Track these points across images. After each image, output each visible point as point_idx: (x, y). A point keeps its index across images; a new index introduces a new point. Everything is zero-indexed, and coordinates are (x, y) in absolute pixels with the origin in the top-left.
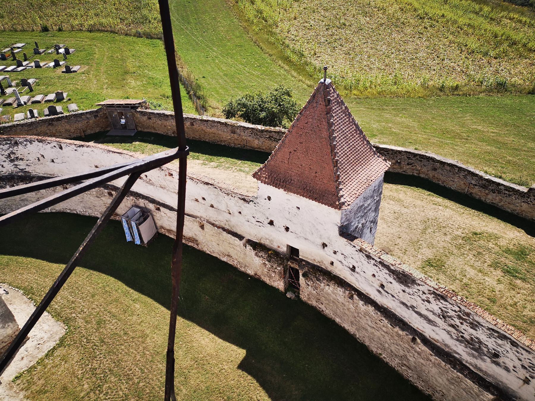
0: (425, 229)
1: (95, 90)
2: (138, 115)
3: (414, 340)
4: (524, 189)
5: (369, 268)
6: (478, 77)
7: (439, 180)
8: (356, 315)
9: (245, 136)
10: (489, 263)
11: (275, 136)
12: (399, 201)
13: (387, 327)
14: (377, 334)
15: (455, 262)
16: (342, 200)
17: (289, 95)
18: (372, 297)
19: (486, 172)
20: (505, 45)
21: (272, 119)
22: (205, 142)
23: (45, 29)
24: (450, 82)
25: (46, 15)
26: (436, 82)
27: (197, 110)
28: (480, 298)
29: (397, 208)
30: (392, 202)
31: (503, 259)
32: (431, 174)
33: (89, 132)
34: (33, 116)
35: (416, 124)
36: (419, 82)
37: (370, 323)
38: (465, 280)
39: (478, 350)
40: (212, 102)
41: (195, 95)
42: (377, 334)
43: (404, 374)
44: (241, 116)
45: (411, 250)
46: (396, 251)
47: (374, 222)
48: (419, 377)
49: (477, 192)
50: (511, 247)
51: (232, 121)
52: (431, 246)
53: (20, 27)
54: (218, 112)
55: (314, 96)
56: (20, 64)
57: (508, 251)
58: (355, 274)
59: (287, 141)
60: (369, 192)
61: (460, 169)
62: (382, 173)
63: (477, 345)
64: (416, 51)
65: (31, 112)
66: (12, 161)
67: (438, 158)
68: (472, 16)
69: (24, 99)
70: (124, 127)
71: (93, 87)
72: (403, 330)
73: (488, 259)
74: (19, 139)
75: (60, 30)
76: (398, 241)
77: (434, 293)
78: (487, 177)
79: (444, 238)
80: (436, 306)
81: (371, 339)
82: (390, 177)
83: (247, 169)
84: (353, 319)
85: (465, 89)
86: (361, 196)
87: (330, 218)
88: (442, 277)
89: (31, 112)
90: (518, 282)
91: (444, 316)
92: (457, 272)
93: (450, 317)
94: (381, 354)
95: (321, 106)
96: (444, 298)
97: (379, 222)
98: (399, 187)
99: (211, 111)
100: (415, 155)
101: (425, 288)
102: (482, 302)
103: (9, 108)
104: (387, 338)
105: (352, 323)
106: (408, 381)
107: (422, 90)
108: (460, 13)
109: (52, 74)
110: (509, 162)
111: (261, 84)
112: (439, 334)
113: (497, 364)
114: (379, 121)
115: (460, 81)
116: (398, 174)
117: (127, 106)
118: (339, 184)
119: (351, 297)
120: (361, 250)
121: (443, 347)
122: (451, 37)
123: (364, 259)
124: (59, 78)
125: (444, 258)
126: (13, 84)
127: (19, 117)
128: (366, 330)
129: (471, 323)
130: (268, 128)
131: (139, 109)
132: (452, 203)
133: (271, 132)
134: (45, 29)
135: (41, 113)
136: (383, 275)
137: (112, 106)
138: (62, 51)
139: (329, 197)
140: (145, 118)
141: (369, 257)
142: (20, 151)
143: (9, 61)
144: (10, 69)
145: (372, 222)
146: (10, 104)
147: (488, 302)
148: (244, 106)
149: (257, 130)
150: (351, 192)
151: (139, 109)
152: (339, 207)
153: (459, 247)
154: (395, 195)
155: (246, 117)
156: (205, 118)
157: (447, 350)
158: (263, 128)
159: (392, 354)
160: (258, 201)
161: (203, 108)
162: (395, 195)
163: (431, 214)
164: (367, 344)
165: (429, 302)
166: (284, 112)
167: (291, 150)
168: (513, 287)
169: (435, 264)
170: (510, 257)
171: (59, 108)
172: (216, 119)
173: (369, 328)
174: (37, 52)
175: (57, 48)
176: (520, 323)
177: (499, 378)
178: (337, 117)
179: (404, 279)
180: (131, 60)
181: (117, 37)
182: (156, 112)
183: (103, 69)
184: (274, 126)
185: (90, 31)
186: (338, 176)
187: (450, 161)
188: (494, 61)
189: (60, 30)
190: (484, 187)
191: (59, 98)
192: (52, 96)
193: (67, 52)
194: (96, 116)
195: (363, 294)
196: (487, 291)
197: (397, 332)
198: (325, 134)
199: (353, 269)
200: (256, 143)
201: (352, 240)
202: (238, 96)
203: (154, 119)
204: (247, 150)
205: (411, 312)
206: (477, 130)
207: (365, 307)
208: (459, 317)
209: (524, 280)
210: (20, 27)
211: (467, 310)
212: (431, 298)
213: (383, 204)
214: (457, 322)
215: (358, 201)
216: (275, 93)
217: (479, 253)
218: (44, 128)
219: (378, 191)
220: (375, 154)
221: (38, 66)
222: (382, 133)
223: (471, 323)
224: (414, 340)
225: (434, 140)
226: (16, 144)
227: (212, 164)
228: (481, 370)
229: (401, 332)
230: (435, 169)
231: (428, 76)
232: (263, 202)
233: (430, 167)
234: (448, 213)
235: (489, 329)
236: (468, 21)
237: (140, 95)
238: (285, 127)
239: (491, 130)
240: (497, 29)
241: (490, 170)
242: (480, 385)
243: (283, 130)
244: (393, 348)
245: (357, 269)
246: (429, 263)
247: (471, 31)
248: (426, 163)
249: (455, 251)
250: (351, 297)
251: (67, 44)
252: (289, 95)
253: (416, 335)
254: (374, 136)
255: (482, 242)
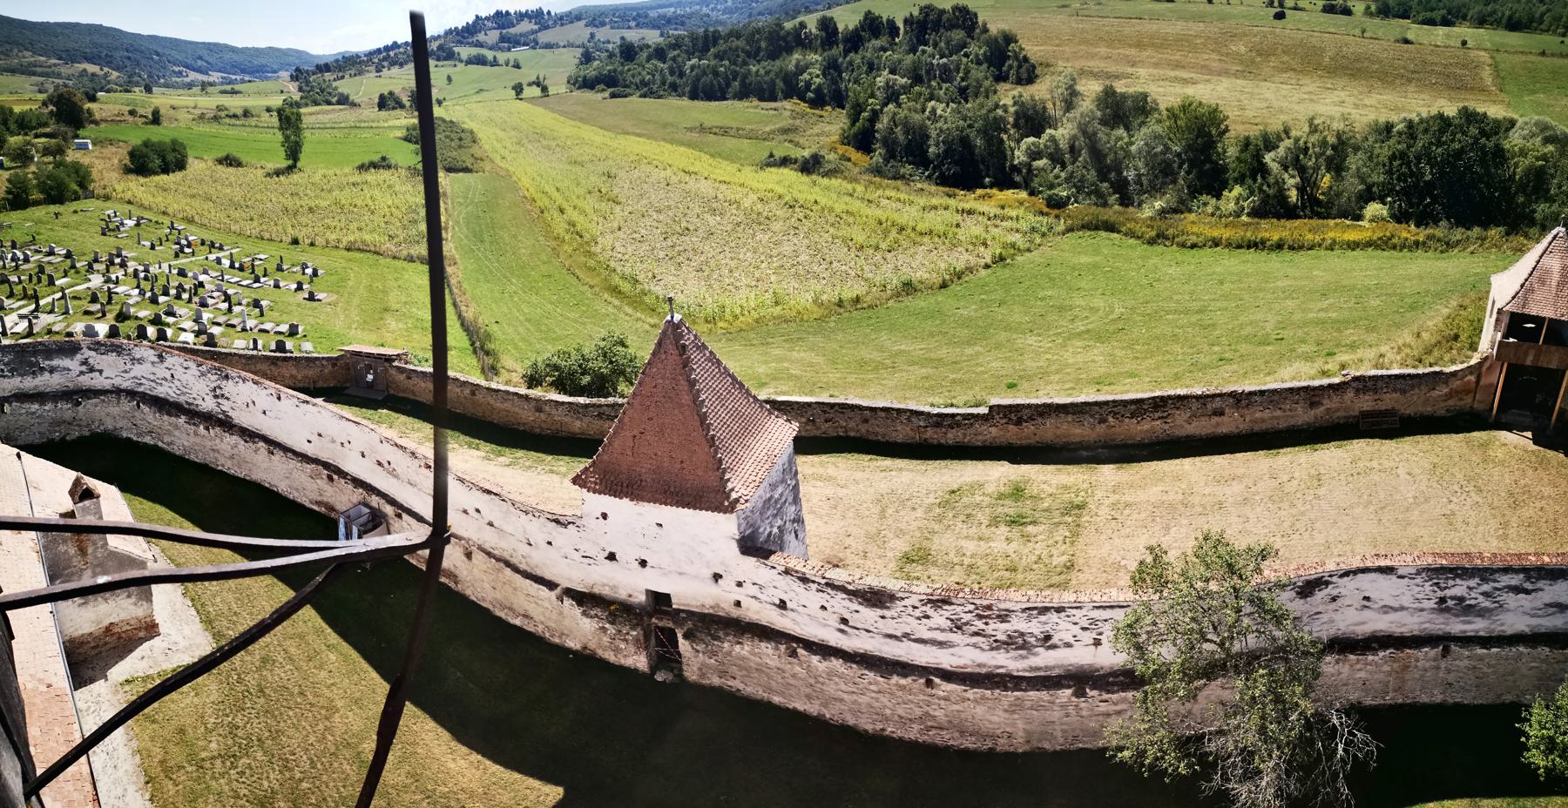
0: (883, 511)
1: (335, 330)
2: (393, 372)
3: (929, 683)
4: (984, 410)
5: (812, 598)
6: (878, 279)
7: (876, 434)
8: (812, 681)
9: (559, 415)
10: (986, 522)
11: (608, 411)
12: (829, 479)
13: (876, 683)
14: (864, 700)
15: (943, 543)
16: (734, 496)
17: (624, 345)
18: (833, 643)
19: (932, 405)
20: (894, 234)
21: (601, 386)
22: (491, 424)
23: (295, 242)
24: (848, 294)
25: (300, 224)
26: (829, 296)
27: (483, 371)
28: (996, 575)
29: (830, 491)
30: (819, 484)
31: (1000, 509)
32: (863, 428)
33: (320, 384)
34: (255, 348)
35: (820, 360)
36: (809, 297)
37: (843, 687)
38: (967, 561)
39: (1025, 646)
40: (507, 361)
41: (482, 348)
42: (864, 700)
43: (938, 740)
44: (551, 384)
45: (873, 550)
46: (851, 559)
47: (798, 520)
48: (962, 733)
49: (931, 434)
50: (1002, 489)
51: (536, 392)
52: (900, 533)
53: (267, 236)
54: (516, 378)
55: (659, 344)
56: (257, 280)
57: (1001, 496)
58: (789, 613)
59: (626, 419)
60: (775, 475)
61: (899, 411)
62: (790, 441)
63: (1020, 641)
64: (796, 254)
65: (255, 341)
66: (216, 397)
67: (865, 403)
68: (848, 199)
69: (250, 323)
70: (370, 385)
71: (338, 325)
72: (905, 676)
73: (983, 517)
74: (232, 372)
75: (312, 244)
76: (848, 541)
77: (930, 601)
78: (936, 411)
79: (914, 515)
80: (940, 618)
81: (856, 712)
82: (803, 445)
83: (563, 469)
84: (808, 690)
85: (868, 298)
86: (765, 484)
87: (719, 530)
88: (933, 571)
89: (255, 341)
90: (1030, 528)
91: (958, 627)
92: (952, 555)
93: (966, 624)
94: (883, 730)
95: (673, 357)
96: (946, 602)
97: (807, 517)
98: (824, 458)
99: (504, 375)
100: (832, 406)
101: (914, 600)
102: (1000, 579)
103: (231, 330)
104: (885, 700)
105: (809, 697)
106: (948, 748)
107: (816, 309)
108: (834, 196)
109: (291, 300)
110: (954, 381)
111: (580, 333)
112: (965, 655)
113: (1054, 647)
114: (766, 362)
115: (858, 289)
116: (815, 438)
117: (380, 357)
118: (724, 471)
119: (793, 654)
120: (787, 572)
121: (978, 670)
122: (832, 230)
123: (798, 587)
124: (299, 305)
125: (925, 543)
126: (244, 302)
127: (240, 344)
128: (842, 700)
129: (999, 616)
130: (595, 400)
131: (396, 364)
132: (906, 461)
133: (600, 406)
134: (295, 242)
135: (266, 345)
136: (840, 604)
137: (358, 354)
138: (309, 271)
139: (712, 497)
140: (402, 377)
141: (804, 580)
142: (229, 387)
143: (246, 274)
144: (245, 283)
145: (794, 521)
146: (233, 326)
147: (1007, 574)
148: (556, 367)
149: (577, 405)
150: (747, 479)
151: (396, 364)
152: (731, 509)
153: (940, 519)
154: (821, 471)
155: (560, 385)
156: (494, 386)
157: (984, 671)
158: (588, 401)
159: (904, 721)
160: (583, 522)
161: (492, 370)
162: (821, 471)
163: (883, 487)
164: (851, 721)
165: (927, 617)
166: (619, 372)
167: (636, 432)
168: (1027, 538)
169: (916, 558)
170: (1007, 502)
171: (289, 345)
172: (512, 389)
173: (845, 696)
174: (280, 269)
175: (304, 266)
176: (1056, 579)
177: (1066, 662)
178: (700, 369)
179: (877, 598)
180: (396, 292)
181: (382, 260)
182: (419, 369)
183: (356, 301)
184: (606, 397)
185: (348, 250)
186: (720, 461)
187: (881, 404)
188: (889, 256)
189: (312, 244)
190: (938, 425)
191: (293, 331)
192: (284, 328)
193: (315, 273)
194: (334, 365)
195: (814, 643)
196: (1000, 561)
197: (897, 685)
198: (686, 399)
199: (782, 605)
200: (577, 425)
201: (767, 558)
202: (546, 352)
203: (415, 380)
204: (562, 438)
205: (906, 643)
206: (901, 352)
207: (826, 664)
208: (980, 617)
209: (1034, 523)
210: (267, 236)
211: (985, 603)
212: (928, 609)
213: (803, 489)
214: (980, 624)
215: (760, 491)
216: (602, 344)
217: (968, 516)
218: (264, 367)
219: (790, 471)
220: (770, 413)
221: (277, 286)
222: (775, 379)
223: (999, 616)
224: (929, 683)
225: (851, 378)
226: (227, 377)
227: (501, 459)
228: (1039, 669)
229: (903, 681)
230: (866, 421)
231: (819, 288)
232: (592, 523)
233: (858, 419)
234: (906, 477)
235: (1024, 610)
236: (845, 207)
237: (401, 342)
238: (622, 396)
239: (915, 348)
240: (879, 213)
241: (937, 400)
242: (1048, 688)
243: (620, 401)
244: (900, 712)
245: (789, 605)
246: (908, 559)
247: (851, 220)
248: (851, 414)
249: (937, 527)
250: (793, 654)
251: (318, 263)
252: (624, 345)
253: (928, 674)
254: (762, 385)
255: (965, 500)
